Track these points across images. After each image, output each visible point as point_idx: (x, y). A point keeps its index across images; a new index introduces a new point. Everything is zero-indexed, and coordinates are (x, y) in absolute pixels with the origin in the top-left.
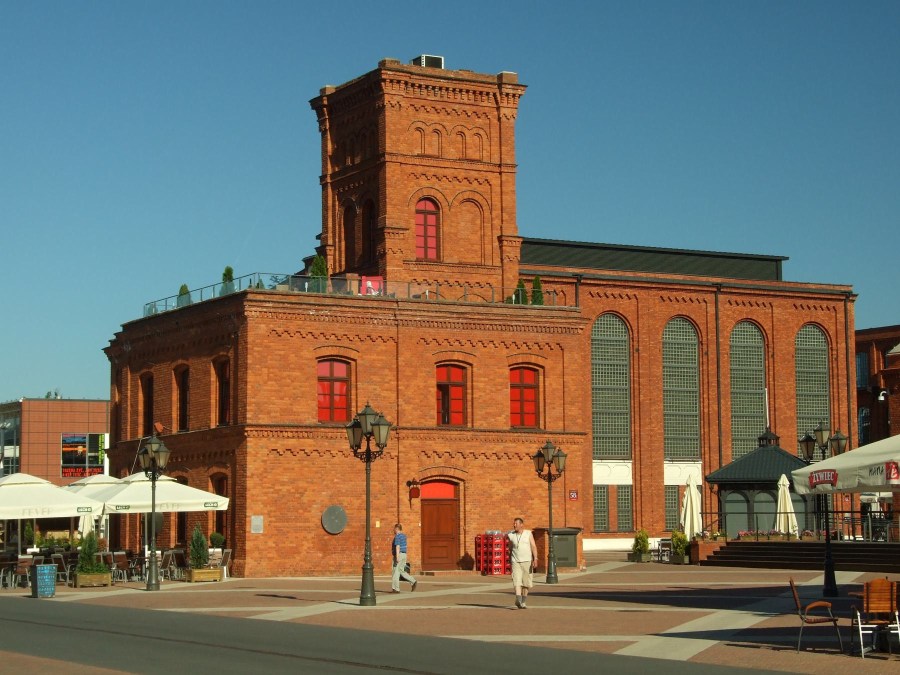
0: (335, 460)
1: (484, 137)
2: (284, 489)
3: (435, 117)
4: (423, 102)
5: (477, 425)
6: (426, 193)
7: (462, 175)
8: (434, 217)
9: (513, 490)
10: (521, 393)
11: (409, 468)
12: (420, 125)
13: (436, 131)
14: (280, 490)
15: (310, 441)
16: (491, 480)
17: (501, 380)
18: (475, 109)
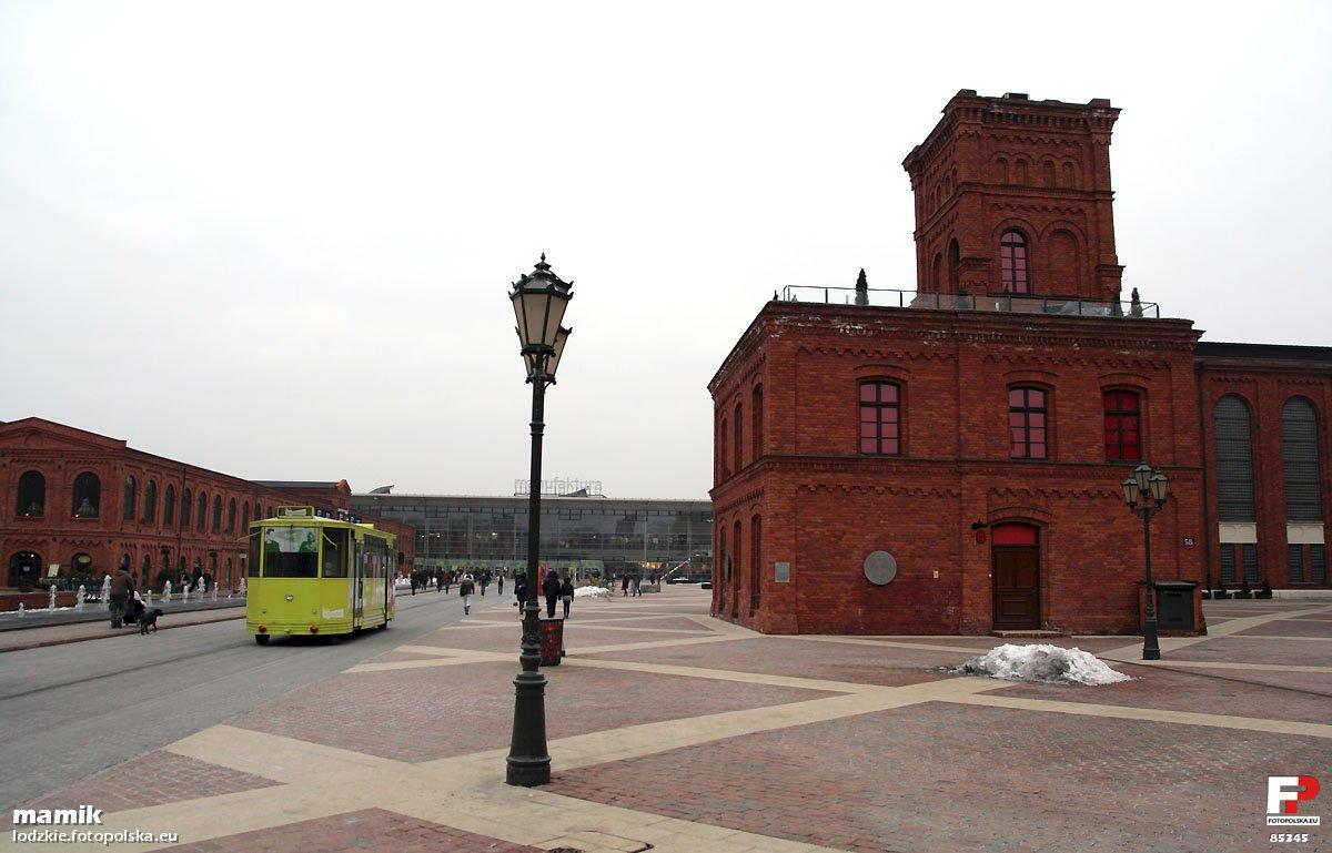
0: (882, 498)
1: (1076, 167)
2: (817, 531)
3: (1019, 147)
4: (1004, 132)
5: (1062, 458)
8: (1023, 249)
9: (1110, 535)
10: (1013, 252)
11: (974, 508)
13: (1021, 162)
14: (812, 533)
15: (850, 476)
16: (1080, 524)
17: (1091, 405)
18: (1063, 137)
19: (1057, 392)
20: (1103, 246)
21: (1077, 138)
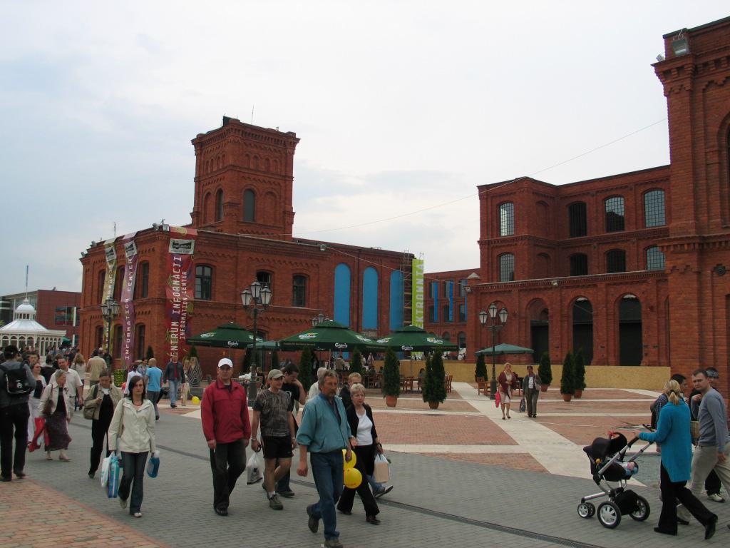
6: (249, 187)
7: (267, 180)
12: (247, 153)
13: (255, 157)
19: (276, 275)
20: (287, 202)
21: (281, 149)
